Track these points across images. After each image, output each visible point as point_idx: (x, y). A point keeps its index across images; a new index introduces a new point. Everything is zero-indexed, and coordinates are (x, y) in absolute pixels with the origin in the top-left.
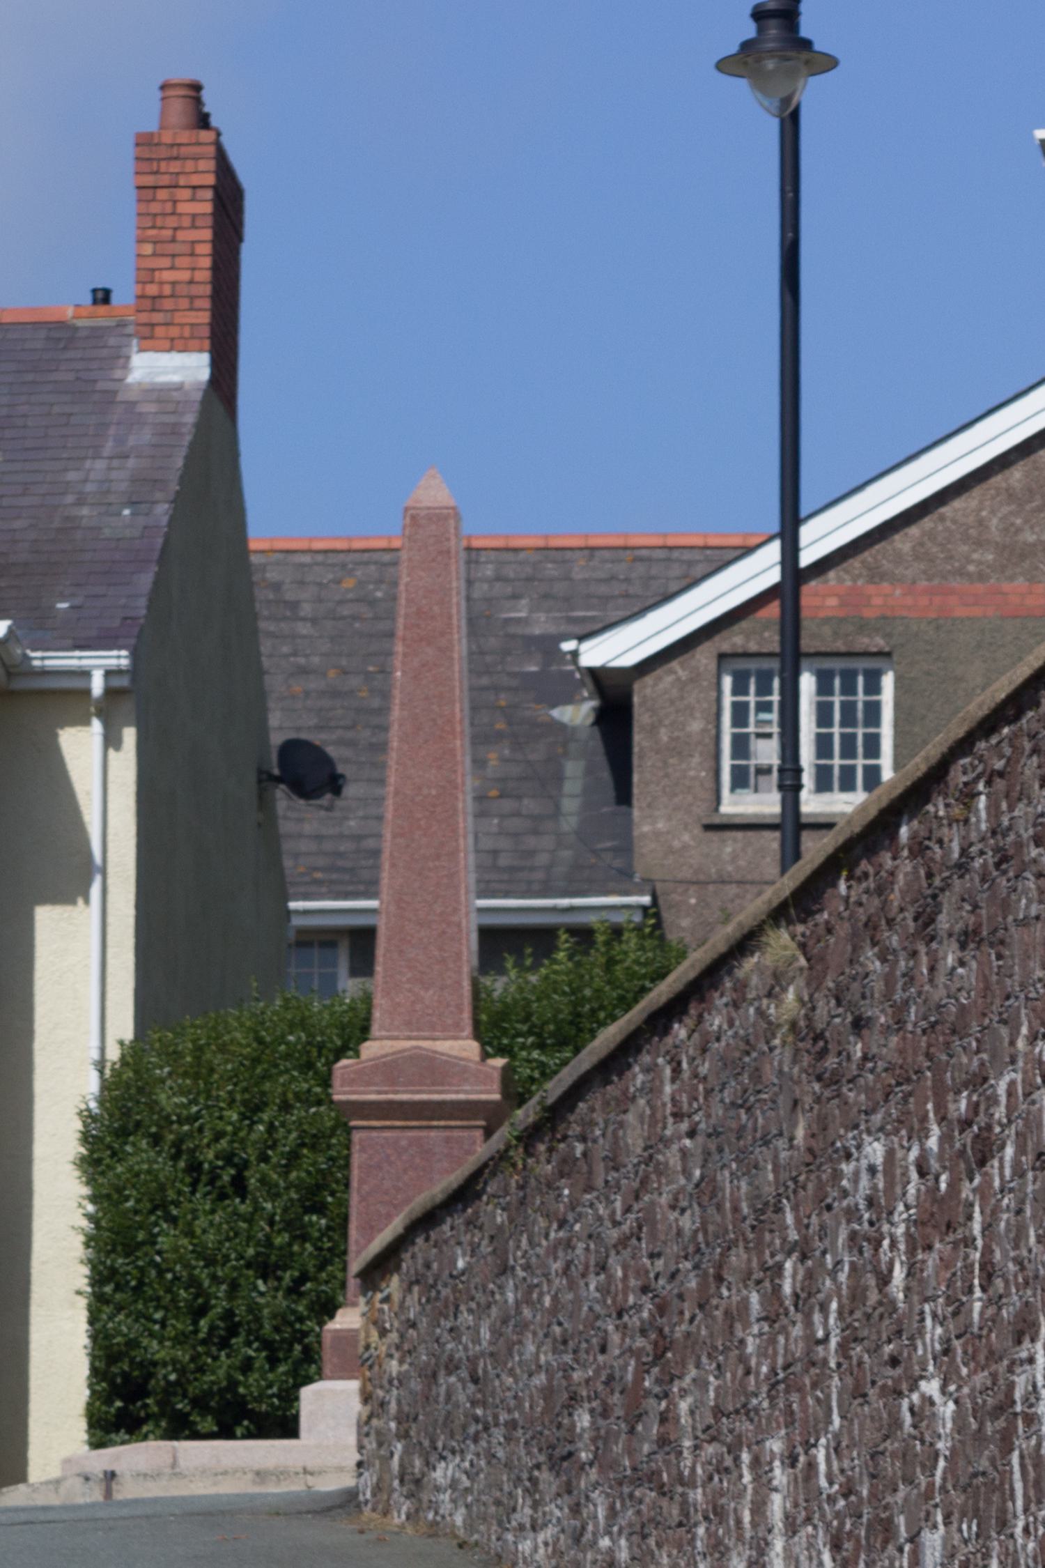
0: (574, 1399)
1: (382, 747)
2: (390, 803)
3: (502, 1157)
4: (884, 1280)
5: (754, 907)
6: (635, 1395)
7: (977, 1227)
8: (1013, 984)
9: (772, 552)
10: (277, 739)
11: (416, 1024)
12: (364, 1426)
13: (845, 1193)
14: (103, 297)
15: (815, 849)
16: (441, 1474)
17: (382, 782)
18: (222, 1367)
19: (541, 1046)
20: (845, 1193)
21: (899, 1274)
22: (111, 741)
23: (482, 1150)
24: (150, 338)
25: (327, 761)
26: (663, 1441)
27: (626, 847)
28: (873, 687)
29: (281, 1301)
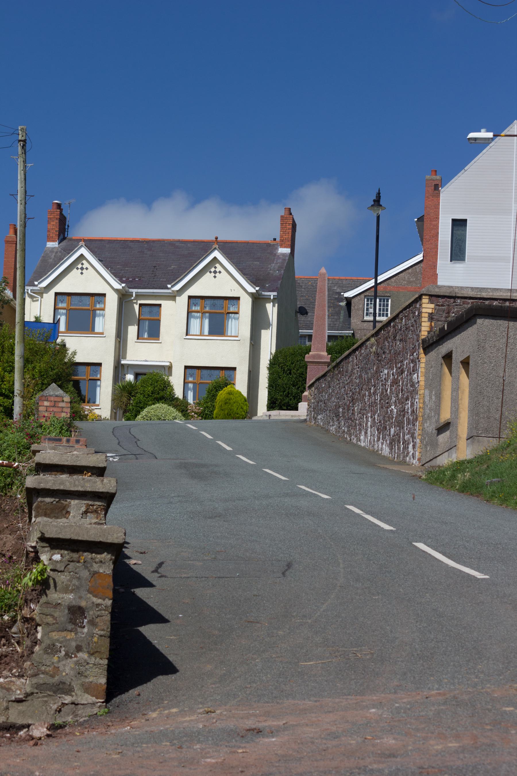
0: (339, 407)
1: (314, 308)
2: (315, 317)
3: (330, 370)
4: (387, 391)
5: (369, 335)
6: (349, 407)
7: (401, 384)
8: (407, 347)
9: (373, 280)
10: (298, 306)
11: (318, 350)
12: (308, 410)
13: (381, 378)
14: (275, 239)
15: (378, 326)
16: (319, 417)
17: (314, 313)
18: (287, 400)
19: (336, 353)
20: (381, 378)
21: (389, 390)
22: (274, 306)
23: (326, 369)
24: (282, 246)
25: (306, 310)
26: (353, 414)
27: (350, 324)
28: (388, 301)
29: (296, 391)
